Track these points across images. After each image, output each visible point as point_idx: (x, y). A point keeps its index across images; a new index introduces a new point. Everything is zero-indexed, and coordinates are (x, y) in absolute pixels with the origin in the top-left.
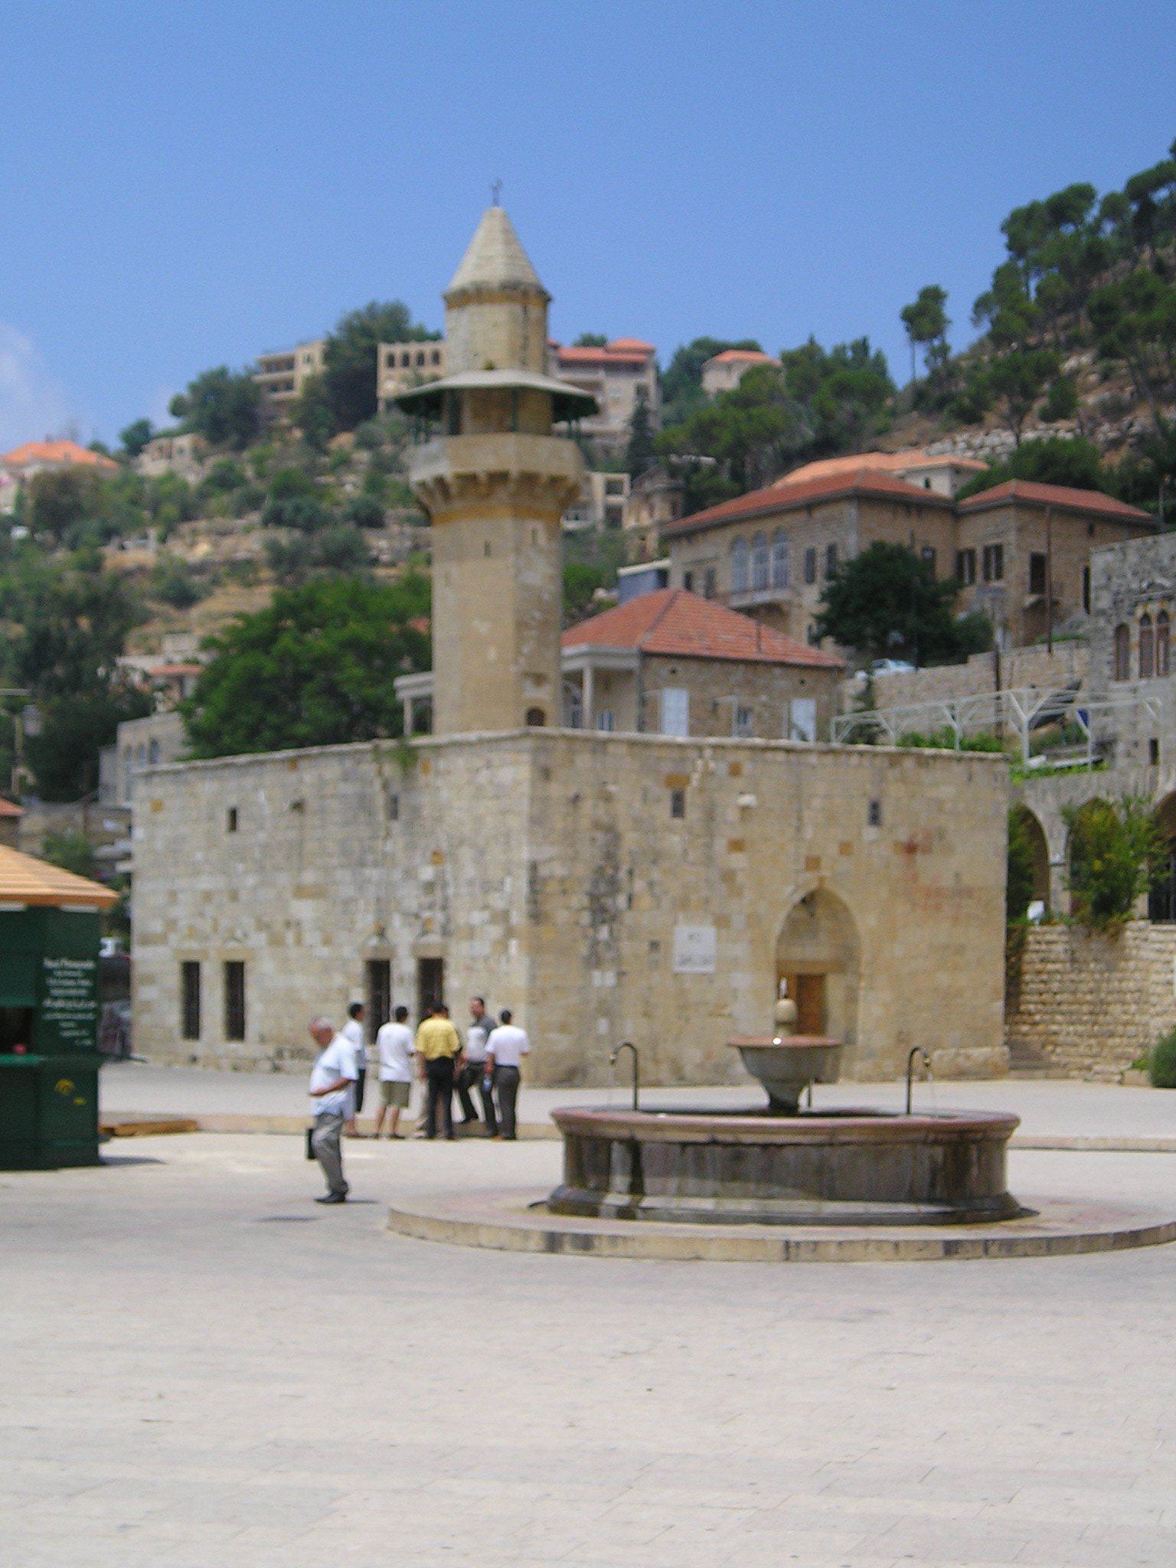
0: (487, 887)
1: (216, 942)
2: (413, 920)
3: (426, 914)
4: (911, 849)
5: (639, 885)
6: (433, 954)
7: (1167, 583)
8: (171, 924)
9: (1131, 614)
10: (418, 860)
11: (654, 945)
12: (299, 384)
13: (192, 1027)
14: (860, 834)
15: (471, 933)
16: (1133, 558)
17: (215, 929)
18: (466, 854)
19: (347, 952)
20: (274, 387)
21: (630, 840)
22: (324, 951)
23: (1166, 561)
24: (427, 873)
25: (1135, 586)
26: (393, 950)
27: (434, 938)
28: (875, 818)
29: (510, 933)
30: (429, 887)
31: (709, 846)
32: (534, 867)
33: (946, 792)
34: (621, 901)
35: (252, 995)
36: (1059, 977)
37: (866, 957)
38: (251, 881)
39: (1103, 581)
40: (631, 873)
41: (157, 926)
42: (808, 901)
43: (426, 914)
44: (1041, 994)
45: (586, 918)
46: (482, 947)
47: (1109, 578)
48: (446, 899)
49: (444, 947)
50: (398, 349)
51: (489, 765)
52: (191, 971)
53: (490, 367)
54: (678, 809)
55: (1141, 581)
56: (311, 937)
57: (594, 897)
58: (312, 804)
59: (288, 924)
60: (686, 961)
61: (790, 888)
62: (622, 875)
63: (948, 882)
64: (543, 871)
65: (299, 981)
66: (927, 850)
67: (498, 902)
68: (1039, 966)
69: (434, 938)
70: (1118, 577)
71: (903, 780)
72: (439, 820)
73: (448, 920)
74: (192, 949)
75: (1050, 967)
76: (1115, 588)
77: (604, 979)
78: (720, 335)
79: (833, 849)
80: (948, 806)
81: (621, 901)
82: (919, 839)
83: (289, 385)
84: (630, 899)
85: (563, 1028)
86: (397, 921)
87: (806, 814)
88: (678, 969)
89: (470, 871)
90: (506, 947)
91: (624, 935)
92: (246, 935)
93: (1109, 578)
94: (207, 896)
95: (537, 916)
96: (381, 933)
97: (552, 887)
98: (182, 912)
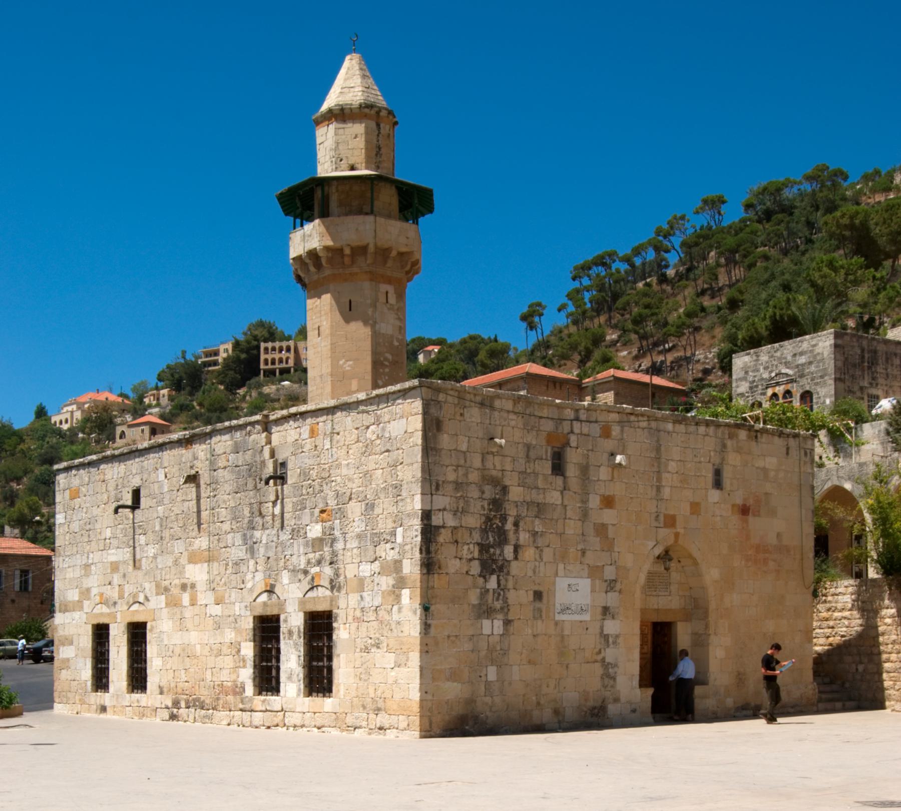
0: (377, 539)
1: (122, 607)
2: (301, 576)
3: (314, 570)
4: (745, 511)
5: (524, 537)
6: (321, 607)
7: (790, 372)
8: (86, 593)
9: (764, 394)
10: (306, 519)
11: (538, 595)
12: (220, 360)
13: (101, 680)
14: (706, 496)
15: (361, 585)
16: (764, 358)
17: (121, 597)
18: (355, 509)
19: (238, 609)
20: (209, 364)
21: (516, 493)
22: (217, 610)
23: (789, 358)
24: (315, 531)
25: (766, 375)
26: (282, 604)
27: (323, 592)
28: (718, 484)
29: (401, 583)
30: (318, 544)
31: (585, 501)
32: (426, 515)
33: (771, 462)
34: (509, 551)
35: (152, 650)
36: (846, 622)
37: (713, 605)
38: (151, 551)
39: (742, 374)
40: (516, 524)
41: (73, 595)
42: (665, 557)
43: (314, 570)
44: (828, 637)
45: (476, 568)
46: (372, 599)
47: (746, 373)
48: (334, 554)
49: (332, 600)
50: (270, 345)
51: (378, 422)
52: (101, 633)
53: (352, 168)
54: (558, 468)
55: (771, 372)
56: (205, 597)
57: (483, 548)
58: (204, 479)
59: (184, 587)
60: (566, 609)
61: (651, 544)
62: (509, 526)
63: (772, 540)
64: (436, 520)
65: (193, 637)
66: (757, 514)
67: (388, 553)
68: (824, 615)
69: (323, 592)
70: (753, 371)
71: (738, 450)
72: (326, 479)
73: (337, 575)
74: (102, 614)
75: (836, 614)
76: (751, 379)
77: (492, 627)
78: (427, 336)
79: (686, 509)
80: (772, 474)
81: (509, 551)
82: (751, 502)
83: (215, 363)
84: (517, 548)
85: (454, 676)
86: (285, 577)
87: (665, 475)
88: (558, 617)
89: (358, 526)
90: (398, 598)
91: (510, 585)
92: (147, 599)
93: (746, 373)
94: (115, 567)
95: (429, 565)
96: (270, 591)
97: (444, 537)
98: (93, 582)
